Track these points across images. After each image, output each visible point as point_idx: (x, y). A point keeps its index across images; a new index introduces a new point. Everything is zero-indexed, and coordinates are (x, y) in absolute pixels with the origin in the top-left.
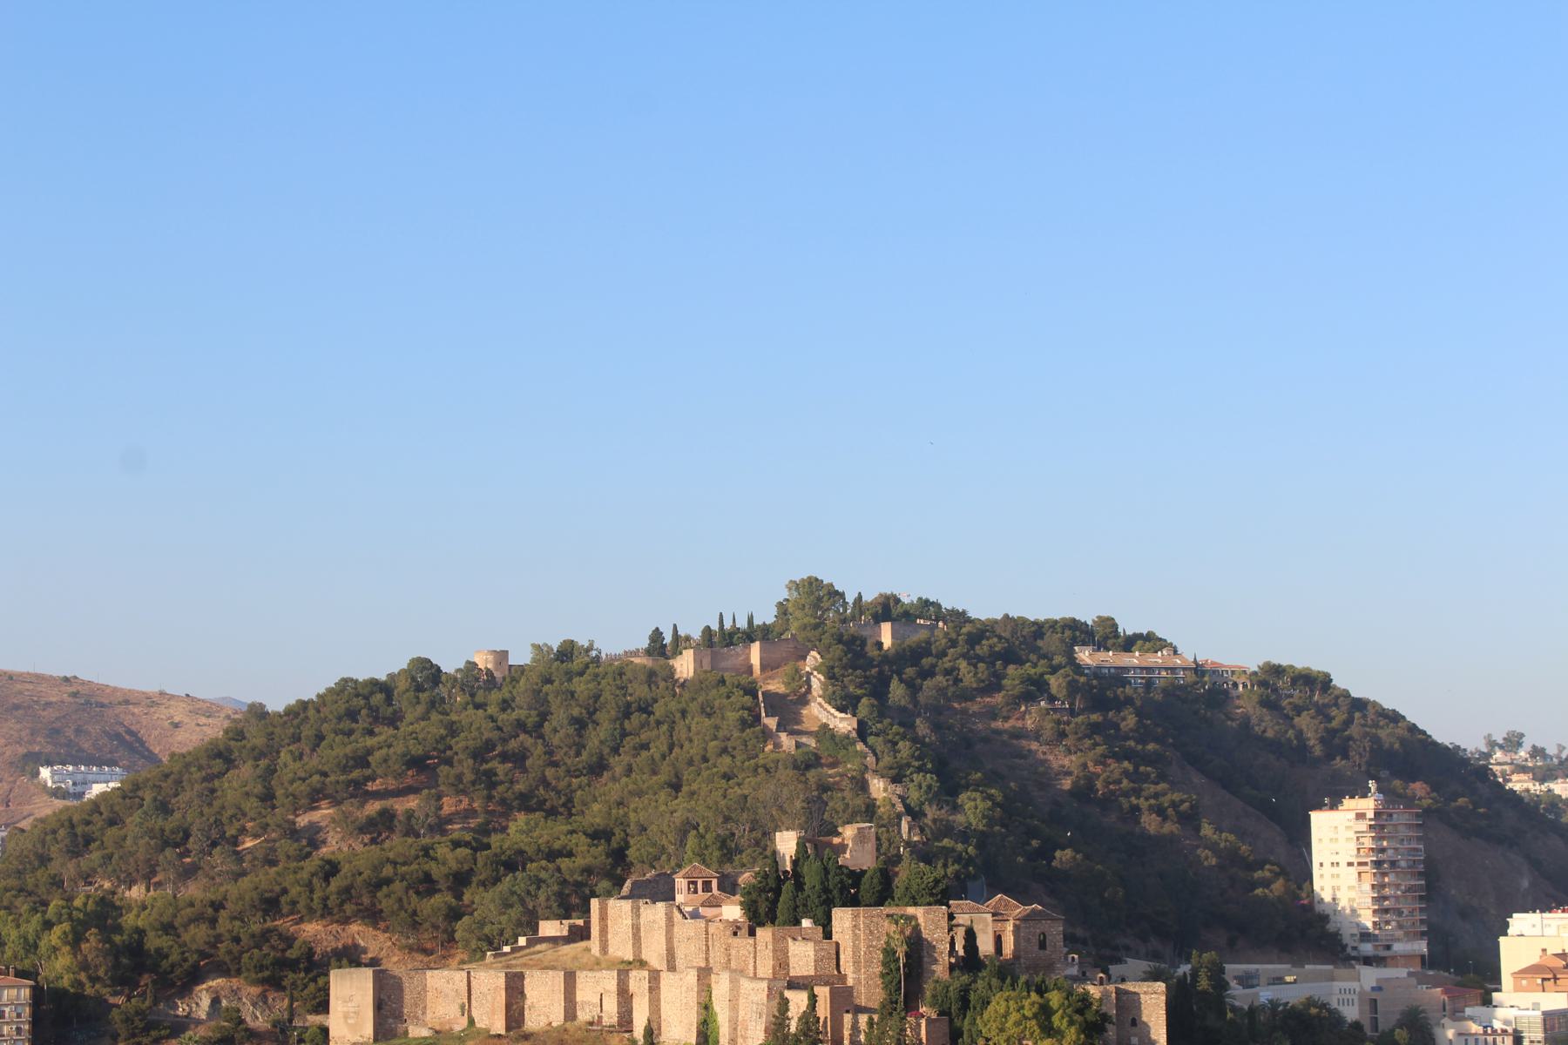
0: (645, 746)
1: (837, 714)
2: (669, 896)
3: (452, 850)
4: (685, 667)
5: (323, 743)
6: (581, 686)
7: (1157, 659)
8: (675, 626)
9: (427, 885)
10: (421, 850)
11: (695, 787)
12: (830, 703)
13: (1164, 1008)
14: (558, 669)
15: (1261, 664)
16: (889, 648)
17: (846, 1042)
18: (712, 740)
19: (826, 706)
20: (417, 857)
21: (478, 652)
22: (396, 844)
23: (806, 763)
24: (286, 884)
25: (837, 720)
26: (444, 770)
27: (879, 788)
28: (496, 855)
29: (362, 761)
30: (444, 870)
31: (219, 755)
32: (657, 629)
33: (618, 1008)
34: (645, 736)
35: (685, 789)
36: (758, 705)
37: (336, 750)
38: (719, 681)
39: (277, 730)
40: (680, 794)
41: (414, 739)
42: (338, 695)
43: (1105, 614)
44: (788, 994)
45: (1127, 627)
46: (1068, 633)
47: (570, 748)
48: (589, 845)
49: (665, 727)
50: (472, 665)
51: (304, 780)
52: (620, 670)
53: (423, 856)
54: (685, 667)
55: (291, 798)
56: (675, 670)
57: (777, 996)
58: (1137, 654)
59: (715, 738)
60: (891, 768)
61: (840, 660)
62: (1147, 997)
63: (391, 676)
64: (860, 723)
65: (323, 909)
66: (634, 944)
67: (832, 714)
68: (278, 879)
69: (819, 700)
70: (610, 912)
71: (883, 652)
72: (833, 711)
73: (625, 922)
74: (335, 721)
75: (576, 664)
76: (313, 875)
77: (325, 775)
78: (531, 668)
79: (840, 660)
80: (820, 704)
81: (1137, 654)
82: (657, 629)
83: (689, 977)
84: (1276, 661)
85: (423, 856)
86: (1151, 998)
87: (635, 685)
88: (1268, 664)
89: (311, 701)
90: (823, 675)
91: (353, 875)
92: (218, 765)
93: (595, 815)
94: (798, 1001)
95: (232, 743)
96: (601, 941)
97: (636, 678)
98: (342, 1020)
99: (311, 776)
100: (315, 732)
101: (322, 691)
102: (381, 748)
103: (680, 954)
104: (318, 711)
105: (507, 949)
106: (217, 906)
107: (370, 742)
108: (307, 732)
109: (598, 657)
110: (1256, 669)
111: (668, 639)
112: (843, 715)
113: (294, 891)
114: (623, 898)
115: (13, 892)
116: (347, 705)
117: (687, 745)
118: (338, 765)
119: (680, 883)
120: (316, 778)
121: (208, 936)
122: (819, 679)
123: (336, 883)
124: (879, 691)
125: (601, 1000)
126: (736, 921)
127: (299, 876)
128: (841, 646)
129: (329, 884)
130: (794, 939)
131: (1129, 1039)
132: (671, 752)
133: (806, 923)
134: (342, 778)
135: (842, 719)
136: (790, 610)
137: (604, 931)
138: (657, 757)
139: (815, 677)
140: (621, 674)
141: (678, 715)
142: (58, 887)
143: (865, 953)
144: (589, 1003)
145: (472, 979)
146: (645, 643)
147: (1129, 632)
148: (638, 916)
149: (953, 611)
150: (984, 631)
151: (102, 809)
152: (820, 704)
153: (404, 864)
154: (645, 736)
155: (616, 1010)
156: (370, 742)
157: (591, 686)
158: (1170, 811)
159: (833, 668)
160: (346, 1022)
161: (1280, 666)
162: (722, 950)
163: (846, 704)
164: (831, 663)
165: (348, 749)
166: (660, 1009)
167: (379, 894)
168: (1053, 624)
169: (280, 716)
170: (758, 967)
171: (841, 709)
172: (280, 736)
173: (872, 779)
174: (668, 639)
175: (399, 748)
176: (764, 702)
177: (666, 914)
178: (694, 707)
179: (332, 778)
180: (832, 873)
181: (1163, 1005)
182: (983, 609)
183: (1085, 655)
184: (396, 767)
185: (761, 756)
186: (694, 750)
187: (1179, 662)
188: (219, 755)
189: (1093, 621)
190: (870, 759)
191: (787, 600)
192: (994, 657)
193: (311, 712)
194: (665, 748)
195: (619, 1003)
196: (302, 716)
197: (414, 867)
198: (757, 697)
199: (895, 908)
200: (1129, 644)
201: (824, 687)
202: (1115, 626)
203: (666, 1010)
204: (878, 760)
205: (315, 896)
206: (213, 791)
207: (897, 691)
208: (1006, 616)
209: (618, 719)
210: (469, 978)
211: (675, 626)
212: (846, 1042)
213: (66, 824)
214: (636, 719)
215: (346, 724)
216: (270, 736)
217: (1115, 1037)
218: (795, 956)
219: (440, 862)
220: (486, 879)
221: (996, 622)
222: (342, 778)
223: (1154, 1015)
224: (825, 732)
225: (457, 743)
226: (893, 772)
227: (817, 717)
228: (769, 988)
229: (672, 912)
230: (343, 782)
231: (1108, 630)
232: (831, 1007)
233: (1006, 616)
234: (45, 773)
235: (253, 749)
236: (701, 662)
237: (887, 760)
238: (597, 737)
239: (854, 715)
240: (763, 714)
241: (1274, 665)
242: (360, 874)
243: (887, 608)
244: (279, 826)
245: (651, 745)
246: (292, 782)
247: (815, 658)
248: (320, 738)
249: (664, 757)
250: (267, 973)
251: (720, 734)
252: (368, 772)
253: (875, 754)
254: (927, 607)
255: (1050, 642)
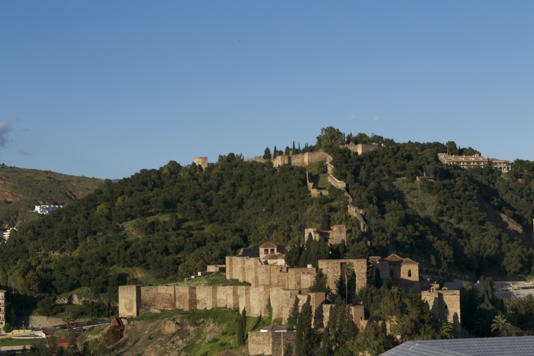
0: (260, 195)
1: (338, 181)
4: (278, 162)
5: (133, 194)
6: (236, 172)
8: (275, 147)
9: (166, 252)
15: (515, 160)
16: (361, 155)
18: (287, 192)
20: (162, 240)
21: (195, 158)
22: (156, 236)
23: (323, 201)
26: (179, 205)
29: (145, 202)
31: (91, 200)
32: (268, 148)
35: (275, 212)
36: (306, 178)
38: (291, 169)
43: (451, 140)
44: (299, 296)
45: (460, 145)
46: (436, 147)
47: (230, 196)
50: (194, 164)
51: (123, 209)
52: (252, 165)
54: (278, 162)
57: (295, 297)
59: (288, 191)
60: (358, 203)
61: (340, 159)
63: (161, 169)
66: (242, 275)
67: (336, 181)
70: (234, 262)
72: (336, 180)
75: (234, 163)
76: (120, 247)
77: (132, 207)
78: (217, 165)
79: (340, 159)
81: (464, 156)
82: (268, 148)
83: (261, 289)
88: (518, 160)
89: (128, 178)
90: (333, 165)
92: (91, 204)
93: (237, 224)
94: (303, 299)
95: (97, 195)
98: (124, 306)
99: (126, 208)
101: (133, 174)
102: (154, 196)
103: (260, 279)
104: (131, 182)
105: (193, 277)
106: (82, 260)
107: (151, 194)
109: (243, 160)
111: (272, 152)
112: (340, 182)
113: (113, 254)
114: (240, 256)
115: (9, 255)
119: (262, 250)
120: (129, 208)
121: (77, 272)
122: (331, 167)
123: (129, 251)
124: (356, 173)
129: (126, 251)
130: (304, 273)
132: (270, 198)
133: (309, 266)
135: (339, 183)
137: (231, 270)
138: (264, 199)
139: (330, 166)
140: (252, 166)
141: (274, 182)
142: (26, 252)
144: (222, 299)
146: (263, 154)
148: (244, 263)
149: (388, 139)
150: (399, 147)
151: (46, 221)
153: (157, 242)
155: (232, 302)
156: (151, 194)
157: (239, 171)
158: (475, 219)
159: (337, 163)
160: (125, 307)
161: (523, 160)
163: (341, 177)
165: (142, 198)
166: (250, 302)
167: (147, 254)
168: (429, 144)
169: (116, 184)
170: (289, 284)
173: (350, 207)
174: (272, 152)
176: (309, 177)
177: (255, 263)
181: (459, 300)
182: (400, 139)
183: (442, 157)
185: (306, 198)
187: (481, 159)
188: (91, 200)
189: (447, 143)
192: (403, 158)
193: (129, 183)
194: (268, 196)
195: (234, 299)
197: (161, 244)
198: (306, 175)
200: (461, 152)
201: (333, 170)
203: (252, 302)
204: (353, 199)
206: (88, 214)
207: (363, 173)
208: (410, 142)
210: (175, 289)
213: (32, 227)
214: (257, 183)
215: (141, 188)
216: (112, 192)
223: (455, 304)
224: (332, 189)
227: (330, 183)
228: (291, 294)
229: (257, 262)
233: (410, 142)
234: (37, 209)
237: (357, 200)
238: (242, 191)
240: (308, 182)
241: (520, 160)
242: (139, 247)
243: (361, 139)
246: (119, 210)
247: (330, 158)
249: (267, 199)
250: (466, 241)
252: (148, 206)
254: (378, 139)
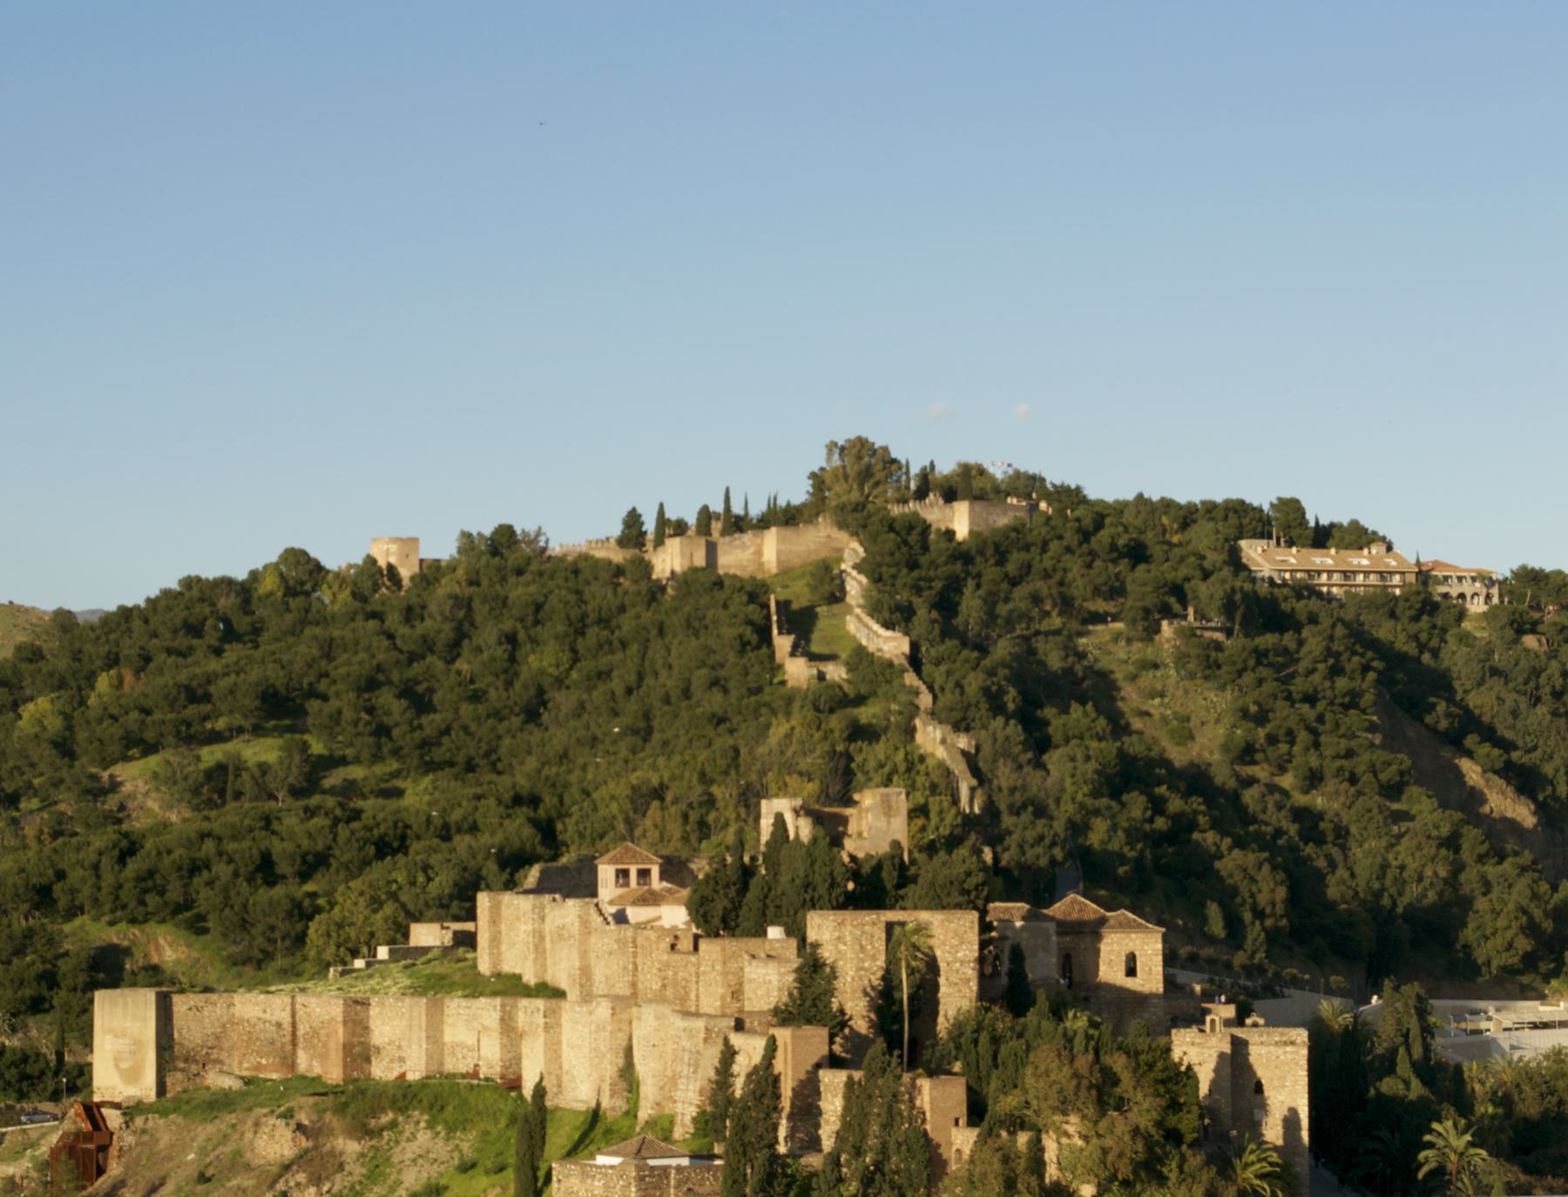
0: (604, 675)
2: (588, 889)
3: (302, 821)
6: (520, 592)
7: (1361, 560)
8: (661, 506)
9: (265, 870)
10: (261, 819)
11: (670, 734)
12: (872, 617)
13: (1306, 1067)
14: (488, 565)
17: (4, 1130)
18: (699, 667)
19: (867, 619)
24: (63, 865)
25: (881, 640)
27: (935, 740)
28: (369, 829)
29: (195, 694)
30: (289, 846)
33: (502, 1054)
34: (604, 661)
35: (656, 737)
36: (768, 617)
37: (170, 675)
39: (88, 648)
40: (648, 744)
41: (275, 661)
42: (175, 598)
43: (1287, 495)
44: (736, 1040)
45: (1319, 512)
46: (1233, 519)
47: (497, 676)
48: (501, 817)
49: (634, 648)
50: (371, 561)
52: (578, 569)
53: (261, 828)
55: (97, 743)
56: (652, 568)
57: (721, 1041)
58: (1333, 551)
59: (703, 664)
60: (952, 710)
62: (1263, 1050)
63: (255, 576)
64: (915, 646)
65: (114, 902)
66: (535, 960)
67: (875, 633)
68: (55, 857)
69: (858, 611)
70: (506, 912)
71: (954, 544)
72: (876, 627)
73: (523, 928)
74: (168, 635)
75: (513, 559)
78: (452, 567)
79: (892, 554)
80: (858, 617)
83: (600, 1010)
84: (1535, 563)
85: (261, 828)
86: (1285, 1053)
87: (595, 587)
90: (867, 577)
91: (159, 853)
93: (521, 777)
94: (750, 1050)
95: (24, 666)
96: (491, 954)
97: (596, 579)
98: (111, 1063)
99: (127, 713)
100: (138, 651)
102: (226, 674)
103: (598, 974)
105: (359, 963)
107: (214, 665)
108: (129, 649)
110: (1508, 574)
111: (650, 525)
112: (889, 633)
116: (186, 612)
117: (664, 673)
118: (166, 697)
120: (135, 715)
122: (860, 583)
123: (133, 866)
124: (946, 605)
125: (478, 1041)
126: (674, 928)
127: (82, 855)
128: (892, 536)
129: (125, 865)
131: (1252, 1113)
132: (639, 687)
134: (171, 716)
135: (887, 639)
136: (828, 482)
137: (495, 940)
139: (854, 578)
140: (576, 572)
141: (654, 632)
143: (853, 979)
144: (462, 1045)
145: (298, 1006)
146: (616, 529)
147: (1324, 521)
148: (543, 919)
149: (1062, 486)
150: (1102, 514)
152: (858, 617)
153: (234, 838)
154: (604, 661)
155: (498, 1056)
156: (214, 665)
157: (532, 589)
159: (879, 565)
160: (117, 1066)
161: (1542, 571)
162: (655, 971)
163: (895, 616)
164: (878, 559)
167: (197, 880)
168: (1210, 508)
170: (702, 996)
171: (888, 625)
172: (90, 656)
174: (650, 525)
175: (254, 674)
177: (580, 917)
178: (676, 620)
179: (157, 716)
180: (819, 863)
181: (1304, 1063)
183: (1254, 552)
184: (246, 702)
185: (767, 690)
186: (669, 682)
187: (1394, 563)
189: (1272, 505)
190: (925, 700)
191: (822, 469)
193: (137, 624)
195: (503, 1046)
196: (123, 627)
197: (246, 844)
199: (901, 912)
200: (1322, 537)
201: (866, 594)
202: (1302, 512)
204: (935, 698)
205: (104, 884)
207: (971, 605)
208: (1140, 496)
209: (566, 635)
210: (293, 1004)
211: (661, 506)
212: (4, 1130)
214: (593, 634)
215: (182, 642)
216: (77, 656)
217: (1229, 1109)
218: (751, 981)
219: (284, 835)
220: (351, 862)
221: (1126, 504)
222: (171, 716)
224: (861, 658)
225: (336, 668)
226: (957, 715)
227: (854, 637)
228: (707, 1029)
230: (170, 721)
231: (1292, 516)
232: (794, 1058)
233: (1140, 496)
235: (51, 674)
236: (692, 555)
237: (947, 699)
238: (541, 660)
239: (907, 634)
241: (1533, 570)
242: (169, 852)
244: (78, 783)
245: (615, 673)
247: (855, 551)
248: (147, 659)
249: (629, 691)
251: (712, 660)
253: (931, 689)
254: (1027, 485)
255: (1202, 537)
